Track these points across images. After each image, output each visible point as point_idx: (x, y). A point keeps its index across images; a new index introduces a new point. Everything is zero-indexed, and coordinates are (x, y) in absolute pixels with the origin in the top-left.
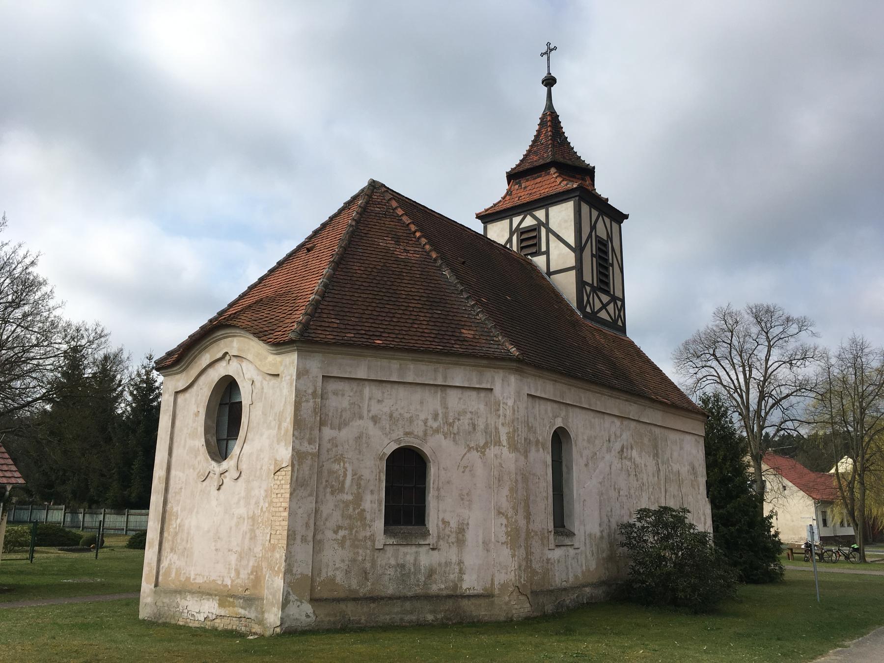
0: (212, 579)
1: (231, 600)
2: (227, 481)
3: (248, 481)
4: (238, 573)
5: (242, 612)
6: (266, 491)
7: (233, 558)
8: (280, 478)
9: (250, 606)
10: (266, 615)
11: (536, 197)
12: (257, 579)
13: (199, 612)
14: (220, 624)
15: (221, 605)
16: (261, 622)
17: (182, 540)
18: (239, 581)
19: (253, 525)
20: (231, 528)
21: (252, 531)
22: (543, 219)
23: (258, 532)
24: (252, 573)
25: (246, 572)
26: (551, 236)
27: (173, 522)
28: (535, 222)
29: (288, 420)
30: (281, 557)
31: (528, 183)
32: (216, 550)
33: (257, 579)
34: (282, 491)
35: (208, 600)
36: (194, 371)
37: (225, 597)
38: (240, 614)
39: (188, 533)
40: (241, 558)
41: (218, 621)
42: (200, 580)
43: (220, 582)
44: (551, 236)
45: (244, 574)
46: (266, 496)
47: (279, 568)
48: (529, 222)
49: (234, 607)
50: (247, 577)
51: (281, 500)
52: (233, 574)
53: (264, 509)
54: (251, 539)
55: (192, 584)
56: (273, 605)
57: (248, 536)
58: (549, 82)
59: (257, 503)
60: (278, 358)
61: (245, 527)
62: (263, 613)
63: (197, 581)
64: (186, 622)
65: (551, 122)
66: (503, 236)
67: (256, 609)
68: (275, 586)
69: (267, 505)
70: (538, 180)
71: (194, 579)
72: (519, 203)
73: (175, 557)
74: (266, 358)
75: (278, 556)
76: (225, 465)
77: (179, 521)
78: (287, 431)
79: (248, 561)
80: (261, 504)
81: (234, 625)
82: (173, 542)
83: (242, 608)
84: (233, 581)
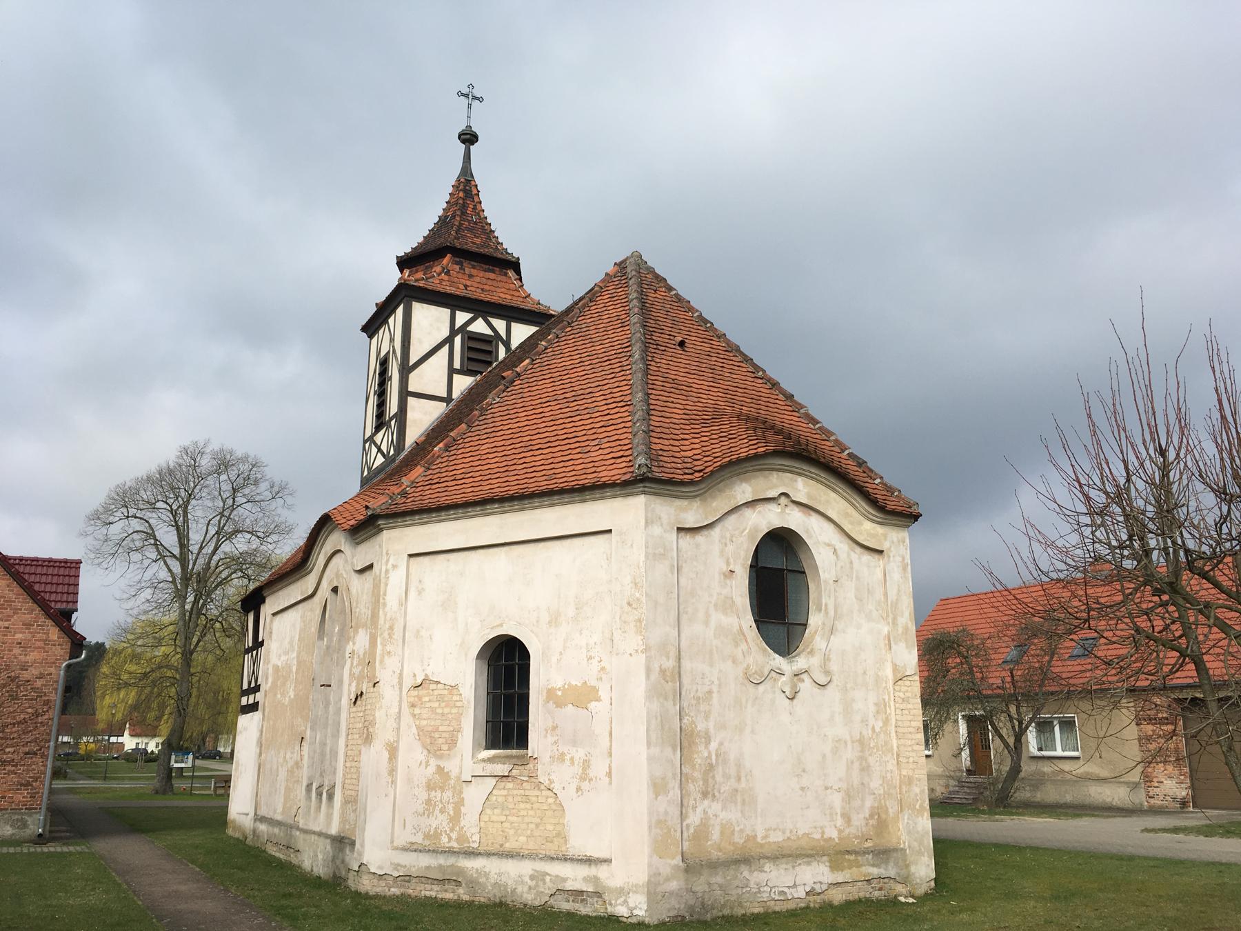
0: (800, 833)
1: (852, 857)
2: (806, 685)
3: (845, 690)
4: (847, 818)
5: (875, 871)
6: (876, 704)
7: (836, 800)
8: (904, 689)
9: (887, 862)
10: (913, 869)
11: (495, 299)
12: (880, 822)
13: (795, 886)
14: (838, 897)
15: (835, 867)
16: (905, 881)
17: (727, 777)
18: (852, 830)
19: (862, 751)
20: (824, 756)
21: (862, 758)
22: (503, 334)
23: (871, 760)
24: (871, 816)
25: (861, 816)
26: (446, 348)
27: (701, 748)
28: (489, 332)
29: (907, 614)
30: (922, 791)
31: (474, 272)
32: (802, 789)
33: (880, 822)
34: (910, 706)
35: (809, 863)
36: (720, 504)
37: (838, 855)
38: (869, 874)
39: (739, 766)
40: (849, 796)
41: (830, 892)
42: (776, 837)
43: (817, 836)
44: (446, 348)
45: (858, 821)
46: (878, 712)
47: (921, 806)
48: (480, 327)
49: (859, 866)
50: (863, 823)
51: (910, 718)
52: (839, 822)
53: (877, 729)
54: (862, 770)
55: (762, 846)
56: (920, 853)
57: (856, 765)
58: (469, 138)
59: (864, 721)
60: (880, 530)
61: (850, 753)
62: (907, 866)
63: (771, 839)
64: (769, 907)
65: (466, 192)
66: (439, 329)
67: (896, 864)
68: (920, 829)
69: (881, 724)
70: (492, 276)
71: (766, 837)
72: (464, 293)
73: (715, 807)
74: (860, 524)
75: (917, 790)
76: (801, 662)
77: (713, 745)
78: (906, 629)
79: (863, 800)
80: (872, 721)
81: (862, 892)
82: (706, 781)
83: (873, 865)
84: (840, 831)
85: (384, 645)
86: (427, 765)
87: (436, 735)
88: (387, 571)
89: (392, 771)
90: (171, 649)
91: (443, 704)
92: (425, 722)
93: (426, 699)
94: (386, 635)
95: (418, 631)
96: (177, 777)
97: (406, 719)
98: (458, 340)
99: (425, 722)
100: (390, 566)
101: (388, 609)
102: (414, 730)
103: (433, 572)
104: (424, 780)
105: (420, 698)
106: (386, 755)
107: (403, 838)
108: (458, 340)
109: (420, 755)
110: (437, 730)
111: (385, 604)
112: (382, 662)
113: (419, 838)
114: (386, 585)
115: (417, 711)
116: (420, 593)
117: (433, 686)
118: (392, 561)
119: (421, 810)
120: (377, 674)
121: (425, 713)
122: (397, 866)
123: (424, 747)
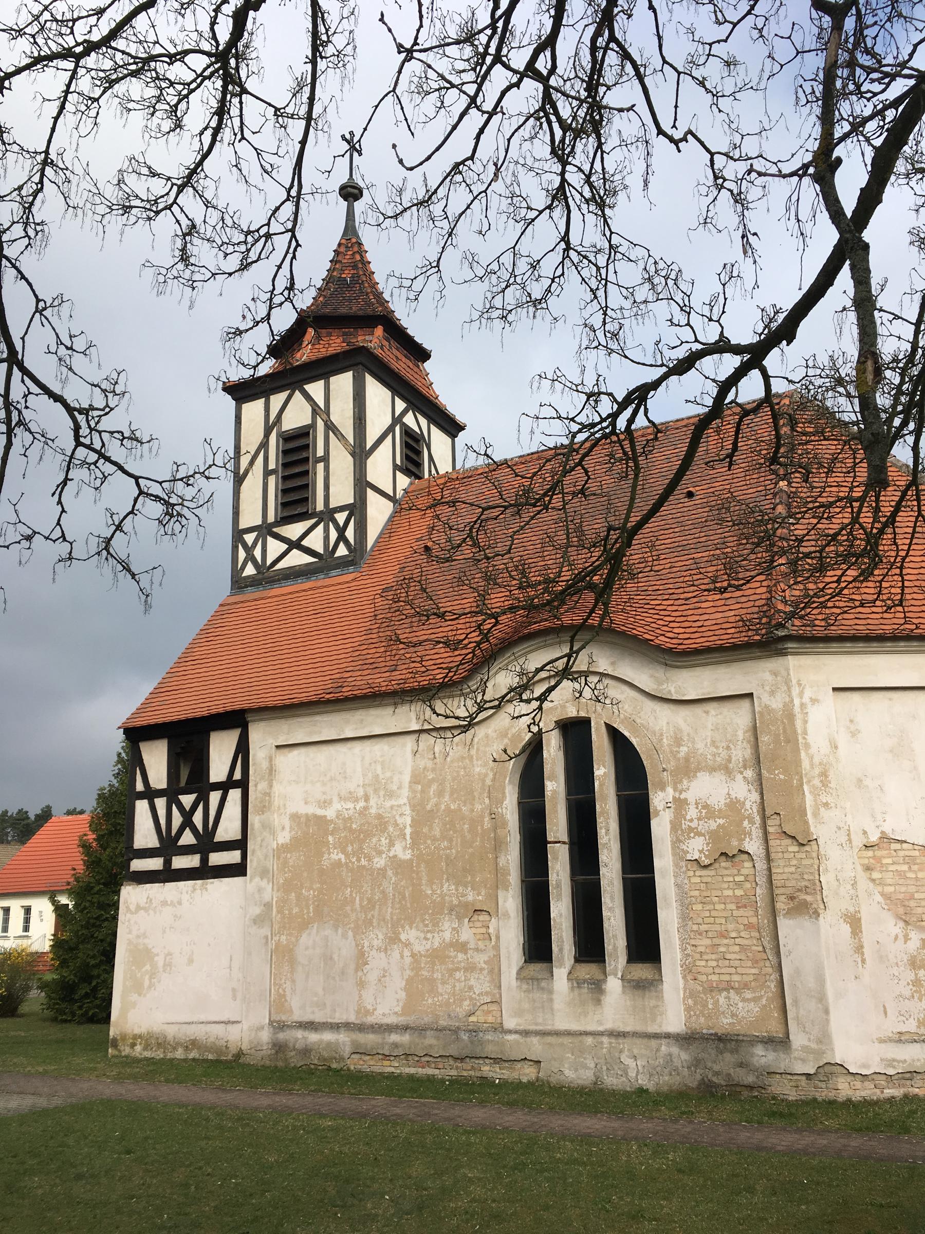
58: (394, 146)
85: (816, 796)
86: (907, 939)
87: (912, 903)
88: (803, 705)
89: (859, 949)
90: (258, 817)
91: (915, 867)
92: (891, 889)
93: (889, 861)
94: (817, 782)
95: (860, 781)
96: (789, 913)
97: (864, 884)
98: (397, 429)
99: (891, 889)
100: (806, 699)
101: (813, 750)
102: (879, 898)
103: (289, 761)
104: (905, 958)
105: (879, 860)
106: (846, 929)
107: (893, 1025)
108: (397, 429)
109: (893, 927)
110: (912, 898)
111: (807, 746)
112: (816, 814)
113: (911, 1026)
114: (806, 722)
115: (876, 875)
116: (854, 734)
117: (895, 846)
118: (808, 694)
119: (908, 993)
120: (812, 829)
121: (889, 878)
122: (891, 1063)
123: (898, 917)
